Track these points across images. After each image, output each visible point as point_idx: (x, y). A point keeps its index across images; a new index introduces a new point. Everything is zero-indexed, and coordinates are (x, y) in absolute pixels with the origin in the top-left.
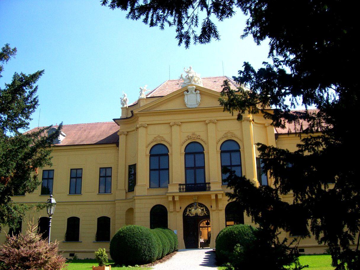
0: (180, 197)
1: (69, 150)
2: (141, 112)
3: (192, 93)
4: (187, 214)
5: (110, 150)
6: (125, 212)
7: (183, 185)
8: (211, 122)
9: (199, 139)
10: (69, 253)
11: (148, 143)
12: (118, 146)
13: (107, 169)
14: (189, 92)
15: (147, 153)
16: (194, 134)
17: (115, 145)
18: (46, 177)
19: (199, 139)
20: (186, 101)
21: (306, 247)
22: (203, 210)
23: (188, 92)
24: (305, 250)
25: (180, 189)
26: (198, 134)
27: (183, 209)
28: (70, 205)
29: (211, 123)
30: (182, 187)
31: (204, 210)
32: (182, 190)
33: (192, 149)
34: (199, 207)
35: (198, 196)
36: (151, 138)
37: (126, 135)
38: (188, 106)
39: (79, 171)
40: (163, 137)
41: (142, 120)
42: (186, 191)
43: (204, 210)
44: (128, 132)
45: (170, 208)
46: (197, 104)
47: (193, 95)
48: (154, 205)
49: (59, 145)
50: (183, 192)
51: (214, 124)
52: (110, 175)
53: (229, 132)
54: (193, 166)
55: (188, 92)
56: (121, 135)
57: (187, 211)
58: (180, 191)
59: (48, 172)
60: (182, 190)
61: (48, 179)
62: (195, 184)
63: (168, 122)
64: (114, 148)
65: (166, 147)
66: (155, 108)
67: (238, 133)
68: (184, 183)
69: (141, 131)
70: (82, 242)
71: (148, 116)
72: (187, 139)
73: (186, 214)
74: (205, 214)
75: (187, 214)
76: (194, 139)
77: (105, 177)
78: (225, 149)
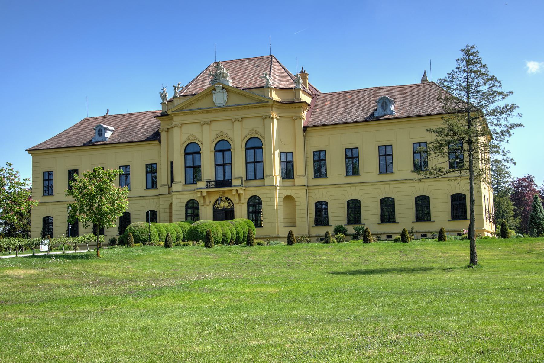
0: (208, 193)
1: (42, 154)
2: (177, 111)
3: (219, 91)
4: (217, 207)
5: (152, 147)
6: (283, 199)
7: (212, 181)
8: (237, 120)
9: (227, 137)
10: (421, 234)
11: (182, 142)
12: (160, 142)
13: (387, 147)
14: (217, 91)
15: (212, 150)
16: (222, 132)
17: (157, 142)
18: (383, 153)
19: (227, 137)
20: (214, 100)
21: (393, 233)
22: (229, 203)
23: (215, 91)
24: (393, 236)
25: (207, 185)
26: (226, 132)
27: (212, 203)
28: (349, 186)
29: (237, 122)
30: (208, 183)
31: (231, 203)
32: (208, 186)
33: (191, 149)
34: (227, 201)
35: (224, 191)
36: (184, 138)
37: (167, 132)
38: (217, 105)
39: (354, 151)
40: (195, 136)
41: (177, 120)
42: (216, 187)
43: (231, 203)
44: (168, 129)
45: (201, 202)
46: (224, 102)
47: (220, 93)
48: (251, 196)
49: (106, 142)
50: (213, 188)
51: (240, 122)
52: (52, 178)
53: (253, 129)
54: (253, 161)
55: (215, 91)
56: (162, 131)
57: (216, 205)
58: (207, 188)
59: (419, 144)
60: (208, 186)
61: (224, 165)
62: (224, 180)
63: (261, 115)
64: (157, 144)
65: (247, 141)
66: (187, 107)
67: (260, 131)
68: (214, 180)
69: (176, 131)
70: (434, 221)
71: (192, 114)
72: (216, 137)
73: (215, 206)
74: (231, 206)
75: (217, 207)
76: (222, 137)
77: (352, 158)
78: (249, 145)
